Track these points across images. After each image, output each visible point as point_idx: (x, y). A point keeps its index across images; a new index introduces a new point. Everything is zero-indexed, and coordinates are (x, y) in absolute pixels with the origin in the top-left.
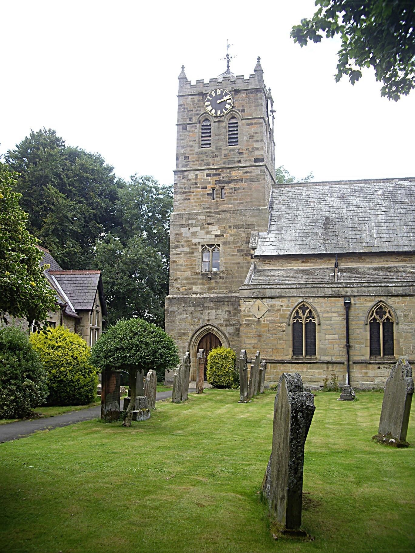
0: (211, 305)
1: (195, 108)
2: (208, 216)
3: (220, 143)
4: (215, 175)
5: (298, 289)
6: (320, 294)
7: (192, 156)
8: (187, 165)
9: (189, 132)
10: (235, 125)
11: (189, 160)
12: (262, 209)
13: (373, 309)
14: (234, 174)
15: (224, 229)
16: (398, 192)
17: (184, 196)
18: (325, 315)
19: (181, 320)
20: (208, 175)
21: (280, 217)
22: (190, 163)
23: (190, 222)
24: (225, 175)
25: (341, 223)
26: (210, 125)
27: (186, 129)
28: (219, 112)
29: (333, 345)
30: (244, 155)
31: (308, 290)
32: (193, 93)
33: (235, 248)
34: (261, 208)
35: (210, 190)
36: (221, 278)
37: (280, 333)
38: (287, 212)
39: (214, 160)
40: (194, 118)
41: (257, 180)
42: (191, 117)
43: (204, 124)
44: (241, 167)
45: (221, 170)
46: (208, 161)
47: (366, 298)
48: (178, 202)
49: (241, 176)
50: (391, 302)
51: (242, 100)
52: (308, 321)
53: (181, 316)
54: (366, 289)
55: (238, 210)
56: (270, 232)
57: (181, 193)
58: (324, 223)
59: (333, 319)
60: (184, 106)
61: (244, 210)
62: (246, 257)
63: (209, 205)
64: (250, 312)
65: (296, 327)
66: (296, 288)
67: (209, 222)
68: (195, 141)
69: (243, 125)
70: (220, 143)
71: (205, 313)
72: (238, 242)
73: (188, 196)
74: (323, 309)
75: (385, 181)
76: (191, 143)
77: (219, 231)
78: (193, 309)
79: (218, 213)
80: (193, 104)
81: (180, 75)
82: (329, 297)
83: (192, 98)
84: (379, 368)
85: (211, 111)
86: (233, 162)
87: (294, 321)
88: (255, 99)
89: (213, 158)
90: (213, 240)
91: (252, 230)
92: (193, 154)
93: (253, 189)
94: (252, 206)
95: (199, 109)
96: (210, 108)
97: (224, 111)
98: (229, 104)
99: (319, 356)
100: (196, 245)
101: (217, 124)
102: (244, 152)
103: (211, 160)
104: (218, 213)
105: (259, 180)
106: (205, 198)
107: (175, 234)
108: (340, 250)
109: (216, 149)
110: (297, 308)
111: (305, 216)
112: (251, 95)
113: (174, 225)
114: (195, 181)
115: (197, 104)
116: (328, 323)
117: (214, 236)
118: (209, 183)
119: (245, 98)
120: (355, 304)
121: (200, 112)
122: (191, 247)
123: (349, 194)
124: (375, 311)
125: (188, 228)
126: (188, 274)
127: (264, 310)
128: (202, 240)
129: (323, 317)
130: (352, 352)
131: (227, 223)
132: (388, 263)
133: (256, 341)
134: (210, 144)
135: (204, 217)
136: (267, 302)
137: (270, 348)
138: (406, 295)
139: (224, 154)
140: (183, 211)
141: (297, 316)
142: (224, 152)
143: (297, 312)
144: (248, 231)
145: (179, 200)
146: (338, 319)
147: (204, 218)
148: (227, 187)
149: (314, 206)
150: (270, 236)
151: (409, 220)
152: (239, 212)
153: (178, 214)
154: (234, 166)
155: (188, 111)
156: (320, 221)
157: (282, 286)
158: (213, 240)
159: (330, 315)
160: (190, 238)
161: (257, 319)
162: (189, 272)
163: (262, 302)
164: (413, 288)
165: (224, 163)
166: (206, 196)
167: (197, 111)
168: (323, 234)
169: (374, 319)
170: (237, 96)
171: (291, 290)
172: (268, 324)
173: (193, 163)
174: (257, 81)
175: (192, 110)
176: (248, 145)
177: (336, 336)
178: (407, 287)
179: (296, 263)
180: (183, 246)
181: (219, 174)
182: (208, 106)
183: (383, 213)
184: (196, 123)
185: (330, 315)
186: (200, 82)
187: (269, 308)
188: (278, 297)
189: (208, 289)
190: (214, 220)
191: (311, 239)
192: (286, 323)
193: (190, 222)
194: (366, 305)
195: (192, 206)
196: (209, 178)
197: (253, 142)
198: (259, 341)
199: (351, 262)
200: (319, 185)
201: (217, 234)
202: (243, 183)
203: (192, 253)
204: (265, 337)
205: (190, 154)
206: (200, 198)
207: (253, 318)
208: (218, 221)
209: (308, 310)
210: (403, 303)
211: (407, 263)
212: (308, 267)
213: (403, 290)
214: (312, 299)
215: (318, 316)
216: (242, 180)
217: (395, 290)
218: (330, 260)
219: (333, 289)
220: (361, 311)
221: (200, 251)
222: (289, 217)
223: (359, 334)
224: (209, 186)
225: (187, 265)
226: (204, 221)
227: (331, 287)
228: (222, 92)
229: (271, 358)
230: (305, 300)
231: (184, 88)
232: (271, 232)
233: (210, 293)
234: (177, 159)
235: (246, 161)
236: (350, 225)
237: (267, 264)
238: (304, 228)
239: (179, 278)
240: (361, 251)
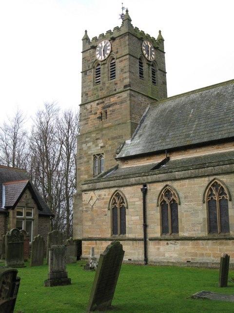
43: (97, 68)
65: (114, 210)
67: (97, 137)
84: (167, 244)
99: (182, 234)
100: (90, 156)
110: (114, 196)
116: (132, 206)
117: (100, 148)
120: (150, 190)
130: (149, 230)
136: (97, 192)
142: (107, 85)
162: (87, 176)
169: (164, 201)
181: (103, 102)
188: (103, 188)
203: (88, 161)
214: (122, 188)
215: (126, 201)
224: (98, 112)
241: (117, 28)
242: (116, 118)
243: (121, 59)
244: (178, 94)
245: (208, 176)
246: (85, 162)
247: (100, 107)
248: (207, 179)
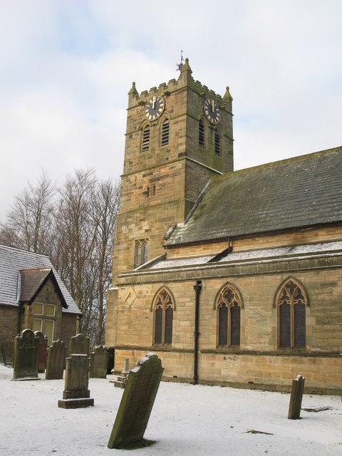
4: (149, 174)
14: (163, 171)
18: (180, 300)
24: (156, 174)
50: (240, 283)
65: (158, 312)
84: (225, 358)
117: (144, 231)
130: (201, 339)
136: (137, 288)
142: (157, 152)
143: (285, 292)
194: (215, 288)
203: (128, 248)
212: (252, 257)
216: (167, 176)
224: (145, 186)
234: (125, 165)
242: (167, 194)
243: (176, 120)
245: (282, 273)
247: (146, 179)
248: (279, 277)
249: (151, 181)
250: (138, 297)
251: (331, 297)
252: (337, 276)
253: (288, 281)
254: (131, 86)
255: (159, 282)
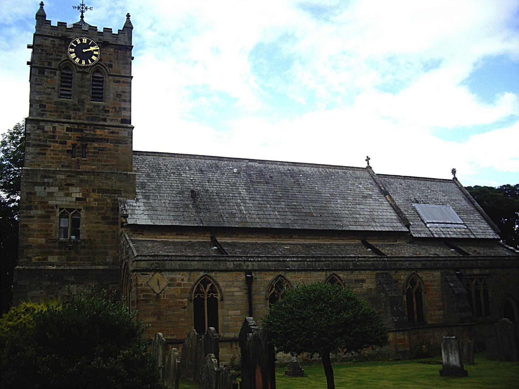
0: (72, 279)
1: (55, 52)
2: (68, 176)
3: (84, 96)
4: (76, 130)
5: (199, 262)
6: (222, 267)
7: (49, 105)
8: (43, 115)
9: (47, 77)
10: (101, 80)
11: (46, 109)
12: (130, 174)
13: (273, 283)
14: (98, 132)
15: (86, 192)
16: (252, 172)
17: (38, 150)
18: (228, 290)
19: (34, 296)
20: (68, 129)
21: (143, 186)
22: (47, 112)
23: (46, 180)
25: (208, 196)
26: (71, 75)
27: (44, 74)
28: (84, 62)
29: (236, 322)
30: (110, 114)
31: (210, 263)
32: (53, 35)
33: (99, 214)
34: (129, 173)
35: (70, 147)
36: (82, 247)
37: (182, 310)
38: (150, 181)
39: (76, 114)
40: (53, 63)
41: (124, 142)
42: (50, 61)
44: (107, 126)
45: (83, 126)
46: (68, 114)
47: (266, 273)
48: (31, 156)
49: (106, 136)
50: (289, 276)
51: (109, 55)
52: (196, 297)
53: (34, 292)
54: (266, 263)
55: (103, 173)
56: (137, 200)
57: (34, 145)
58: (191, 195)
59: (235, 294)
60: (43, 47)
61: (110, 173)
62: (111, 226)
63: (69, 163)
64: (149, 286)
65: (198, 303)
66: (198, 260)
67: (69, 182)
68: (54, 88)
69: (109, 81)
70: (84, 96)
71: (65, 288)
72: (103, 208)
73: (43, 150)
74: (225, 283)
75: (237, 160)
76: (49, 90)
77: (81, 194)
78: (49, 283)
79: (81, 173)
80: (53, 48)
81: (39, 12)
82: (231, 271)
83: (52, 41)
85: (75, 59)
86: (97, 119)
87: (195, 296)
88: (123, 56)
89: (75, 112)
90: (73, 204)
91: (119, 196)
92: (51, 103)
93: (119, 152)
94: (118, 170)
95: (60, 54)
96: (73, 56)
97: (90, 62)
98: (96, 56)
100: (52, 207)
101: (80, 75)
102: (110, 110)
103: (72, 113)
104: (81, 173)
105: (126, 142)
106: (64, 155)
107: (27, 193)
108: (216, 224)
109: (78, 102)
111: (169, 187)
112: (119, 51)
113: (25, 182)
114: (52, 134)
115: (58, 48)
116: (230, 298)
117: (74, 199)
118: (70, 138)
119: (113, 53)
120: (256, 278)
121: (61, 58)
122: (47, 210)
123: (207, 169)
124: (274, 285)
125: (43, 187)
126: (42, 241)
127: (164, 284)
128: (61, 203)
129: (225, 292)
131: (90, 185)
132: (260, 239)
133: (155, 320)
134: (70, 95)
135: (64, 176)
136: (168, 275)
137: (171, 327)
138: (302, 270)
139: (88, 109)
140: (37, 166)
141: (198, 291)
142: (87, 106)
144: (115, 197)
145: (32, 154)
146: (239, 293)
147: (62, 177)
148: (90, 145)
149: (175, 177)
150: (138, 204)
151: (270, 200)
152: (104, 175)
153: (31, 170)
154: (100, 123)
155: (47, 54)
156: (186, 193)
157: (182, 258)
158: (73, 204)
159: (232, 289)
160: (45, 199)
161: (156, 294)
162: (44, 240)
163: (162, 275)
164: (307, 263)
165: (88, 119)
166: (66, 153)
167: (57, 55)
168: (193, 207)
170: (104, 49)
171: (193, 263)
172: (168, 300)
173: (50, 113)
174: (126, 37)
175: (52, 54)
176: (115, 104)
177: (239, 311)
178: (302, 262)
179: (171, 235)
180: (36, 208)
181: (82, 131)
182: (71, 53)
183: (244, 190)
184: (57, 70)
185: (232, 289)
186: (62, 25)
187: (170, 282)
189: (67, 260)
190: (75, 181)
191: (183, 210)
192: (188, 298)
193: (46, 180)
194: (266, 279)
195: (48, 162)
196: (70, 133)
197: (120, 100)
198: (159, 318)
199: (226, 237)
200: (174, 157)
201: (78, 196)
202: (109, 143)
203: (48, 217)
204: (165, 314)
205: (47, 103)
206: (58, 155)
207: (152, 293)
208: (80, 183)
209: (210, 285)
210: (299, 278)
211: (277, 240)
213: (299, 265)
215: (221, 291)
216: (107, 141)
217: (292, 265)
218: (205, 234)
219: (235, 263)
220: (262, 285)
221: (58, 215)
222: (152, 186)
223: (261, 309)
224: (70, 142)
225: (41, 230)
226: (63, 181)
227: (233, 261)
228: (88, 41)
229: (173, 337)
230: (206, 273)
231: (43, 27)
232: (138, 200)
233: (68, 265)
235: (112, 120)
236: (217, 200)
237: (139, 234)
238: (172, 199)
239: (31, 246)
240: (237, 226)
241: (108, 30)
244: (239, 158)
245: (326, 270)
246: (41, 217)
249: (80, 139)
250: (169, 285)
251: (361, 290)
252: (366, 275)
253: (336, 278)
254: (39, 7)
255: (201, 270)
